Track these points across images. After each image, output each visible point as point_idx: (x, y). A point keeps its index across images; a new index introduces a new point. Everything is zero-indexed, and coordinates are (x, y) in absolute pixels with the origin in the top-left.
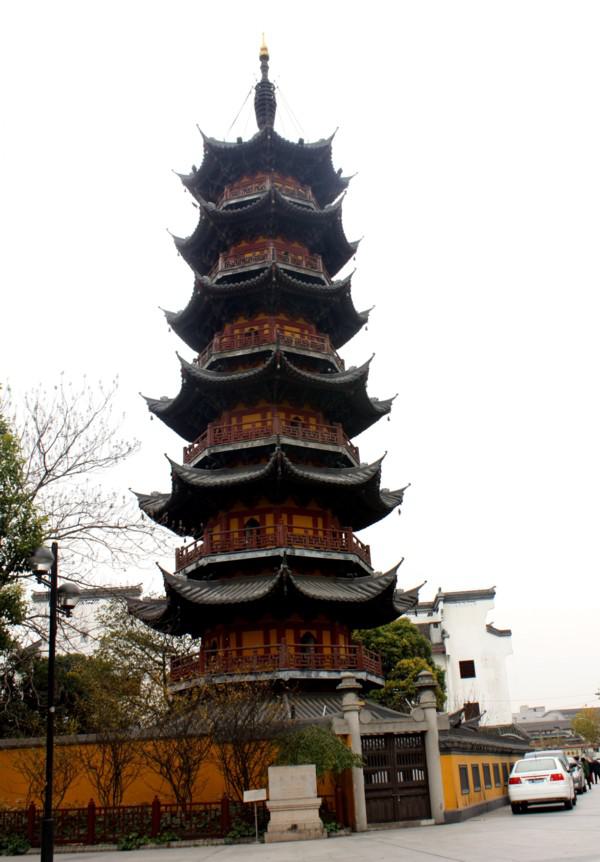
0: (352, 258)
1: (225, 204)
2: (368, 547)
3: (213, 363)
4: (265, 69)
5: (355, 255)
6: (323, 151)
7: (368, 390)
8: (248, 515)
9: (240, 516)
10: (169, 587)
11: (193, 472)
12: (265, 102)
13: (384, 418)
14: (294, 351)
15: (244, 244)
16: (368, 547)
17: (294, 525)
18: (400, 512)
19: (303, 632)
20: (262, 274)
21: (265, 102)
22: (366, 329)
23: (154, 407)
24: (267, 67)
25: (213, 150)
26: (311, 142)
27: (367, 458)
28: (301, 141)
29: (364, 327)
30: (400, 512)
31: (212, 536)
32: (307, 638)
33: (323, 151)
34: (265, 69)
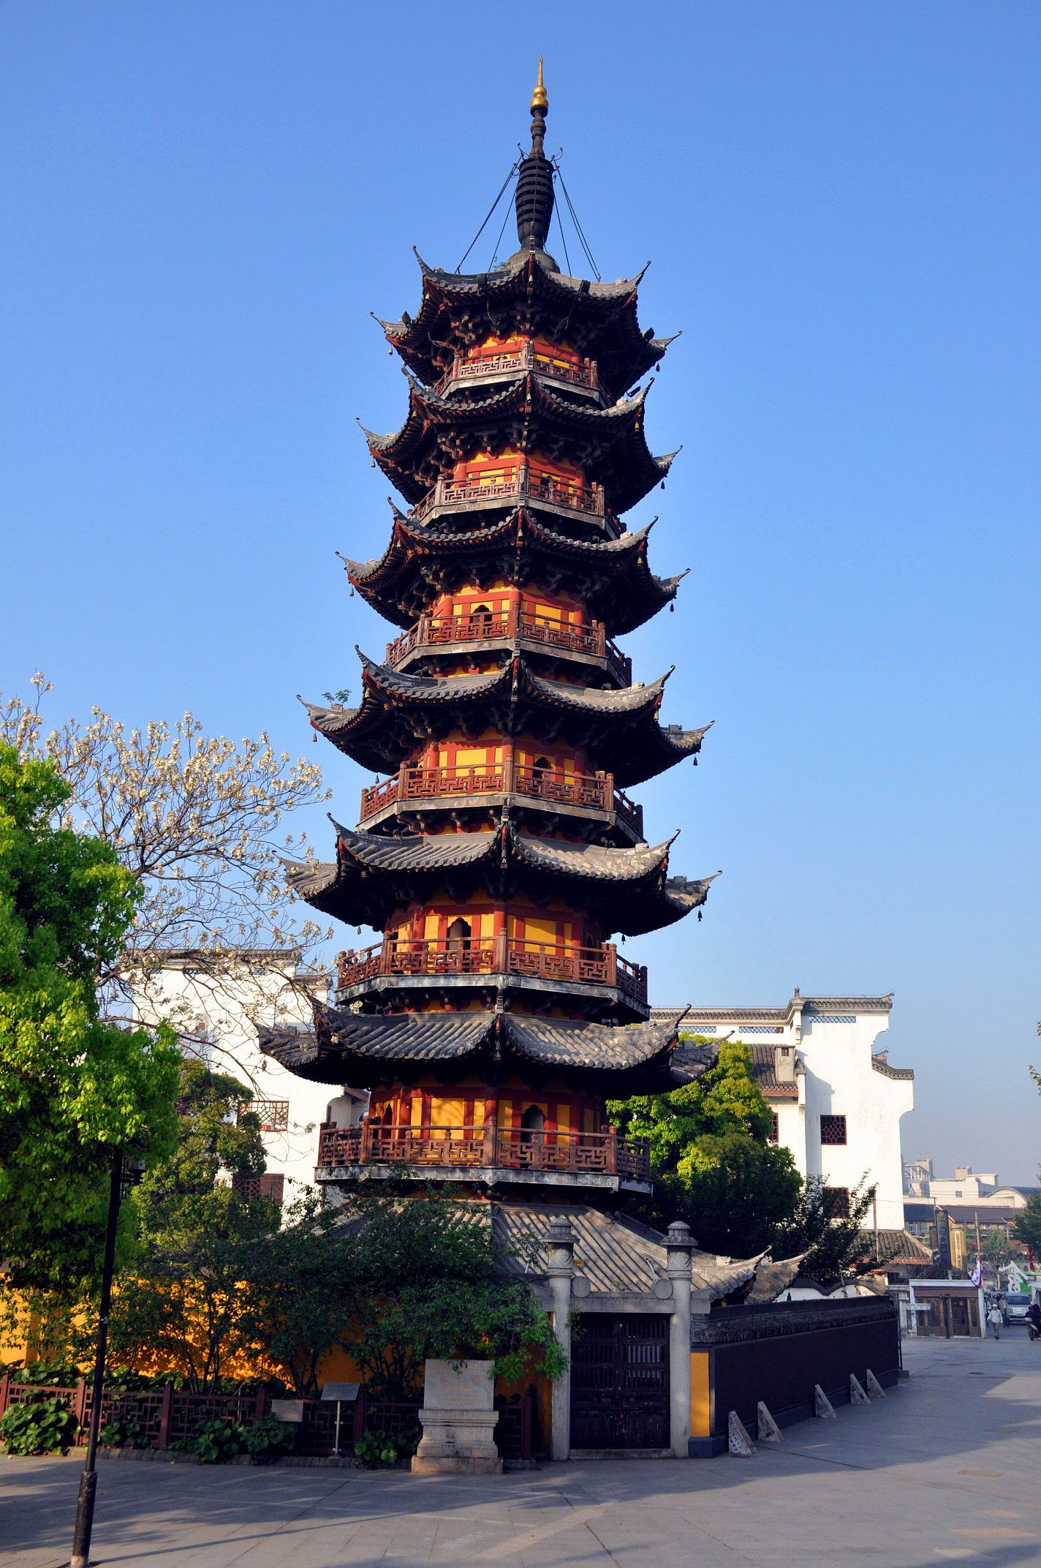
0: (659, 484)
1: (453, 388)
2: (640, 807)
3: (414, 661)
4: (540, 132)
5: (660, 362)
6: (625, 305)
7: (653, 573)
8: (453, 914)
9: (444, 912)
10: (343, 854)
11: (370, 842)
12: (536, 196)
13: (690, 759)
14: (546, 650)
15: (480, 458)
16: (640, 807)
17: (528, 938)
18: (700, 916)
19: (526, 1106)
20: (511, 389)
21: (536, 196)
22: (672, 609)
23: (318, 721)
24: (543, 129)
25: (435, 286)
26: (599, 295)
27: (643, 677)
28: (586, 286)
29: (669, 604)
30: (700, 916)
31: (395, 945)
32: (543, 763)
33: (625, 305)
34: (540, 132)
